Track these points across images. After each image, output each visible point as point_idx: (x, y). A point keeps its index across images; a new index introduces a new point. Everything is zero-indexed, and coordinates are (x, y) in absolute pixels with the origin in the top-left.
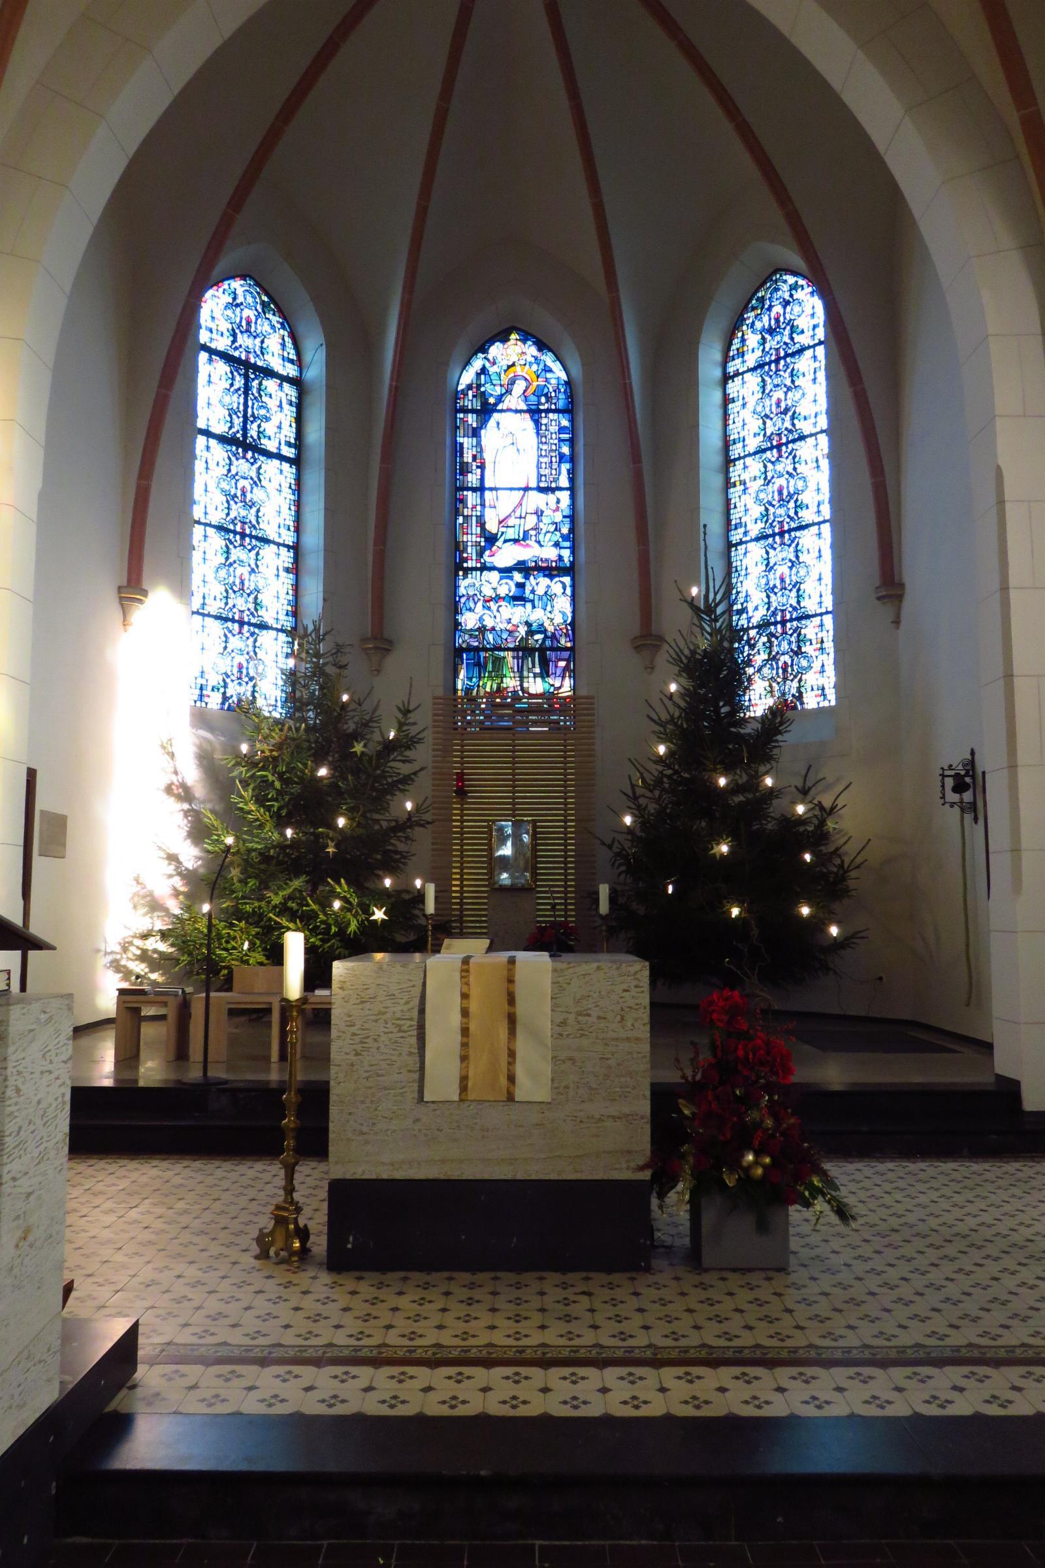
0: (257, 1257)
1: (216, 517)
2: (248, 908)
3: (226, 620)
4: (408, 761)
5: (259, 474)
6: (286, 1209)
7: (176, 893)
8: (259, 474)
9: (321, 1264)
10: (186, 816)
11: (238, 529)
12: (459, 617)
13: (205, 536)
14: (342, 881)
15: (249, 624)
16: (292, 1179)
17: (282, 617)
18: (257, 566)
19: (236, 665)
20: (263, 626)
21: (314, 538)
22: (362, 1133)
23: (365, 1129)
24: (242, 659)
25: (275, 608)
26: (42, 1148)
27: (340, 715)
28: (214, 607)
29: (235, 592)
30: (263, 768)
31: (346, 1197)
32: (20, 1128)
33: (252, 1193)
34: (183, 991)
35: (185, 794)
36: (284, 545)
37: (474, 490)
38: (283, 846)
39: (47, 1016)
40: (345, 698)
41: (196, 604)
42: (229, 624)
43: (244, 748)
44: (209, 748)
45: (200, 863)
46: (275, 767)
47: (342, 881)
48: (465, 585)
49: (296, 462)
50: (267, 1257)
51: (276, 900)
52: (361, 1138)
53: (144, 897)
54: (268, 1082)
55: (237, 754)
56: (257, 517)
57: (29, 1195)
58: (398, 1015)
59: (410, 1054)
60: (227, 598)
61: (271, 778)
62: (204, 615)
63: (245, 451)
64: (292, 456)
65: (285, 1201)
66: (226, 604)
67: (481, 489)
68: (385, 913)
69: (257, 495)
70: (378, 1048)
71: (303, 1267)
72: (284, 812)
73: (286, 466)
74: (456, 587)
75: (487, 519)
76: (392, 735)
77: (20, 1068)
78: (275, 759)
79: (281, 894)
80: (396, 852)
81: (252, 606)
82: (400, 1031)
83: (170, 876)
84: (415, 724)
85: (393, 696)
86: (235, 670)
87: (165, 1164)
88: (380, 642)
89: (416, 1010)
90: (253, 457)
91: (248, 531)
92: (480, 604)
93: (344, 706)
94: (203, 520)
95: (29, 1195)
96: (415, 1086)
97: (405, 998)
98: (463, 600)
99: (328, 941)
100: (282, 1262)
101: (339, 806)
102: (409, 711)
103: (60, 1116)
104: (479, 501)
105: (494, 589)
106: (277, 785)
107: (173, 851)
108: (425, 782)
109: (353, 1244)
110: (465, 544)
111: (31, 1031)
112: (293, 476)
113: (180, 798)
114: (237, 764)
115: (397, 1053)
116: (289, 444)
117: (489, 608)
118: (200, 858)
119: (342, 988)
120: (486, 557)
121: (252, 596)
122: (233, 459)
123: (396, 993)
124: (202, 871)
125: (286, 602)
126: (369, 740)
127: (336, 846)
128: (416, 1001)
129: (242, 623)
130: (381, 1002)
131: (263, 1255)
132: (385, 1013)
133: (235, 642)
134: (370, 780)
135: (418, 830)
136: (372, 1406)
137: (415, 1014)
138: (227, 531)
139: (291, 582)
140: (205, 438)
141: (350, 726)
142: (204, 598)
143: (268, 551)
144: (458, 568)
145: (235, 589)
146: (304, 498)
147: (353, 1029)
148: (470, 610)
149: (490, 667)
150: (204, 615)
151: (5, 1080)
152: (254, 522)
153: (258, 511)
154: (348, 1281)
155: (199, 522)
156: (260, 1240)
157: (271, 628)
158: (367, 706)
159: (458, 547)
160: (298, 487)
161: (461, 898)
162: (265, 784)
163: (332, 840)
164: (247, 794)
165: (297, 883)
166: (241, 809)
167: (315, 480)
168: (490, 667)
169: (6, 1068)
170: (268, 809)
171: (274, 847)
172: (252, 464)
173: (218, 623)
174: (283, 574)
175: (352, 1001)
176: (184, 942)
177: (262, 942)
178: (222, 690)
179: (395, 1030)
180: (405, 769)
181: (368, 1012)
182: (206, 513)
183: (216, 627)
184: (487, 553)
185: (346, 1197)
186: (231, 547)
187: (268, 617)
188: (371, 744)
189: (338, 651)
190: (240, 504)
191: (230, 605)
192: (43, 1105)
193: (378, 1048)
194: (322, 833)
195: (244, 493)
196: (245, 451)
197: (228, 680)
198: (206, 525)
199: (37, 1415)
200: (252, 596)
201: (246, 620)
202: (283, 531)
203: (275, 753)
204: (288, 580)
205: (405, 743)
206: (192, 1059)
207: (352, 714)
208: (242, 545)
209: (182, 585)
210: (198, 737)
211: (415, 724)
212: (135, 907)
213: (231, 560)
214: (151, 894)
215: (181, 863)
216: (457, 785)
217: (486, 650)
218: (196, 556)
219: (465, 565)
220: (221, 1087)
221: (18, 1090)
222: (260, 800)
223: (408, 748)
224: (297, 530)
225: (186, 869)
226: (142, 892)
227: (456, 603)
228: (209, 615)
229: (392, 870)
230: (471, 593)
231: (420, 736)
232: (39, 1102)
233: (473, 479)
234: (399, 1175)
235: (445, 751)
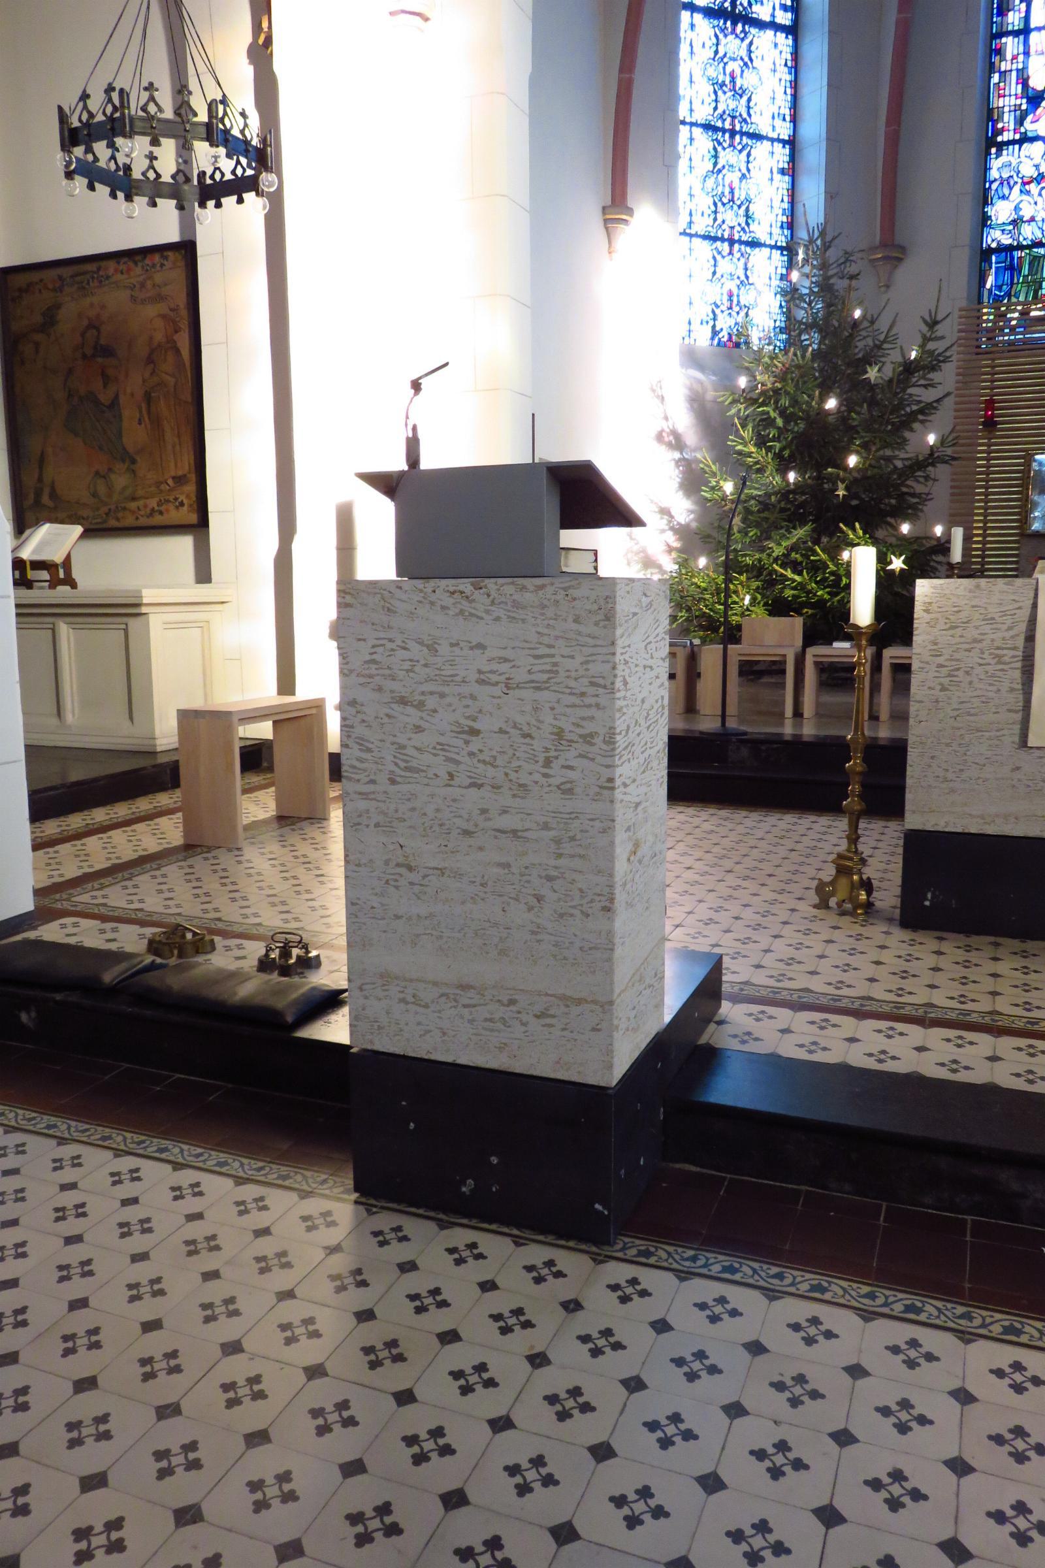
0: (815, 906)
1: (703, 113)
2: (748, 560)
3: (715, 239)
4: (932, 386)
5: (750, 51)
6: (851, 859)
7: (670, 549)
8: (750, 51)
9: (890, 920)
10: (678, 466)
11: (727, 126)
12: (988, 209)
13: (691, 139)
14: (857, 525)
15: (741, 242)
16: (857, 828)
17: (776, 231)
18: (749, 170)
19: (725, 291)
20: (754, 244)
21: (814, 127)
22: (946, 780)
23: (950, 776)
24: (732, 285)
25: (768, 223)
26: (646, 755)
27: (851, 335)
28: (702, 225)
29: (724, 204)
30: (763, 404)
31: (922, 849)
32: (628, 727)
33: (789, 844)
34: (691, 643)
35: (677, 443)
36: (779, 140)
37: (1015, 34)
38: (786, 493)
39: (649, 599)
40: (857, 314)
41: (682, 224)
42: (719, 243)
43: (743, 382)
44: (700, 390)
45: (692, 516)
46: (776, 402)
47: (857, 525)
48: (997, 166)
49: (792, 30)
50: (827, 907)
51: (778, 551)
52: (944, 785)
53: (637, 553)
54: (781, 735)
55: (733, 389)
56: (749, 108)
57: (638, 805)
58: (998, 643)
59: (1012, 690)
60: (715, 212)
61: (772, 414)
62: (691, 236)
63: (734, 24)
64: (788, 23)
65: (848, 850)
66: (715, 220)
67: (1025, 32)
68: (904, 562)
69: (747, 80)
70: (971, 683)
71: (871, 921)
72: (786, 453)
73: (781, 36)
74: (986, 169)
75: (1031, 71)
76: (913, 355)
77: (626, 657)
78: (776, 392)
79: (784, 544)
80: (913, 495)
81: (742, 220)
82: (999, 663)
83: (663, 531)
84: (942, 338)
85: (909, 308)
86: (726, 297)
87: (691, 811)
88: (892, 250)
89: (1022, 637)
90: (743, 31)
91: (738, 128)
92: (1017, 189)
93: (855, 324)
94: (688, 120)
95: (638, 805)
96: (1017, 729)
97: (1009, 622)
98: (994, 186)
99: (837, 594)
100: (853, 914)
101: (851, 441)
102: (936, 323)
103: (660, 722)
104: (1021, 49)
105: (1037, 166)
106: (780, 422)
107: (664, 505)
108: (945, 415)
109: (931, 901)
110: (1001, 110)
111: (635, 614)
112: (789, 50)
113: (670, 446)
114: (734, 401)
115: (994, 688)
116: (784, 8)
117: (1028, 193)
118: (692, 512)
119: (927, 611)
120: (1028, 125)
121: (743, 208)
122: (721, 36)
123: (996, 616)
124: (694, 525)
125: (780, 212)
126: (884, 363)
127: (847, 489)
128: (1023, 627)
129: (732, 242)
130: (977, 628)
131: (823, 905)
132: (980, 641)
133: (725, 266)
134: (886, 413)
135: (941, 467)
136: (857, 1058)
137: (1020, 642)
138: (715, 129)
139: (786, 186)
140: (689, 13)
141: (861, 345)
142: (691, 214)
143: (761, 150)
144: (991, 143)
145: (725, 200)
146: (801, 82)
147: (941, 660)
148: (1004, 197)
149: (1025, 271)
150: (691, 236)
151: (614, 668)
152: (745, 115)
153: (749, 100)
154: (928, 942)
155: (683, 123)
156: (820, 888)
157: (764, 245)
158: (883, 324)
159: (990, 116)
160: (796, 65)
161: (983, 550)
162: (768, 422)
163: (843, 481)
164: (747, 434)
165: (800, 533)
166: (740, 453)
167: (816, 49)
168: (1025, 271)
169: (614, 654)
170: (769, 449)
171: (776, 493)
172: (742, 40)
173: (706, 243)
174: (777, 177)
175: (939, 627)
176: (682, 597)
177: (763, 598)
178: (711, 323)
179: (993, 662)
180: (929, 396)
181: (958, 640)
182: (691, 110)
183: (704, 249)
184: (1030, 118)
185: (922, 849)
186: (719, 149)
187: (760, 231)
188: (885, 369)
189: (847, 260)
190: (729, 94)
191: (719, 221)
192: (646, 706)
193: (971, 683)
194: (831, 474)
195: (733, 78)
196: (734, 24)
197: (717, 311)
198: (692, 124)
199: (648, 1040)
200: (743, 208)
201: (736, 237)
202: (778, 122)
203: (778, 385)
204: (784, 182)
205: (931, 363)
206: (702, 712)
207: (864, 333)
208: (732, 145)
209: (667, 195)
210: (689, 377)
211: (942, 338)
212: (629, 564)
213: (719, 166)
214: (644, 551)
215: (672, 517)
216: (986, 415)
217: (1020, 247)
218: (683, 165)
219: (999, 139)
220: (742, 739)
221: (625, 683)
222: (761, 442)
223: (933, 368)
224: (794, 120)
225: (678, 523)
226: (635, 548)
227: (986, 191)
228: (696, 235)
229: (911, 518)
230: (1005, 176)
231: (948, 354)
232: (643, 701)
233: (1014, 19)
234: (991, 830)
235: (967, 376)
